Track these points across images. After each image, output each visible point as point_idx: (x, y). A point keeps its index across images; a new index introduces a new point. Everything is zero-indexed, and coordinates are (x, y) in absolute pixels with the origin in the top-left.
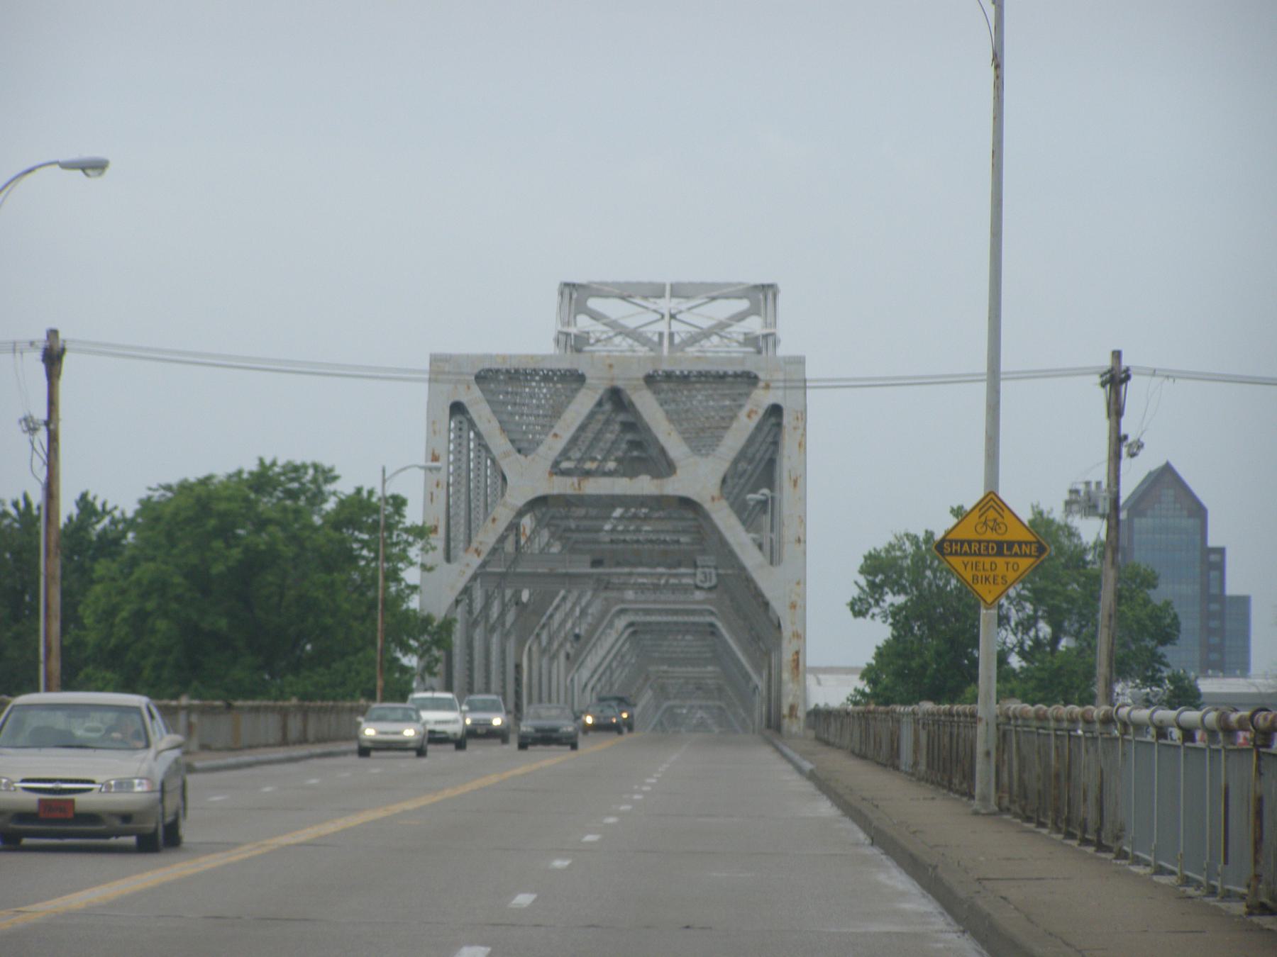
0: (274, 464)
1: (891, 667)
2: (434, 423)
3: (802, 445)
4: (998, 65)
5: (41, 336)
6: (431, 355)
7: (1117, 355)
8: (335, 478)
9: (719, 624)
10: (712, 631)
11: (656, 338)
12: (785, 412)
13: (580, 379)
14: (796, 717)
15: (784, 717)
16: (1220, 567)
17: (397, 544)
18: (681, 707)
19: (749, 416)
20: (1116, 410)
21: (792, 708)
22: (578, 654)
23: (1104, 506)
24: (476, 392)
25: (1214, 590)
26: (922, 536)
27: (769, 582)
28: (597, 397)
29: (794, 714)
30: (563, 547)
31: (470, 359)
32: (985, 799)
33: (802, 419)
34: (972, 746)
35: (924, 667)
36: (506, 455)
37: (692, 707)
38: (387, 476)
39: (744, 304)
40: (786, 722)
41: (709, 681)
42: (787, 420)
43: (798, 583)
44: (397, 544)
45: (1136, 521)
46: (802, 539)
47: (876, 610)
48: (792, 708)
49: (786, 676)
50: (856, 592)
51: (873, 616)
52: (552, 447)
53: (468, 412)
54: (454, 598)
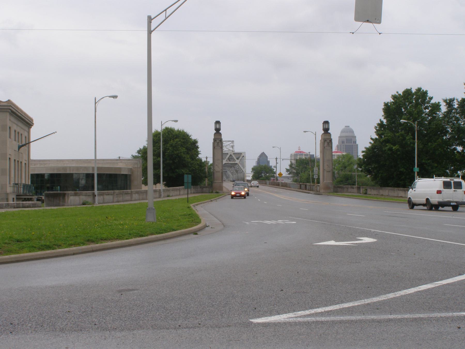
5: (206, 157)
7: (276, 157)
13: (228, 154)
16: (269, 163)
20: (276, 161)
23: (276, 167)
25: (269, 165)
34: (128, 160)
38: (162, 124)
39: (231, 142)
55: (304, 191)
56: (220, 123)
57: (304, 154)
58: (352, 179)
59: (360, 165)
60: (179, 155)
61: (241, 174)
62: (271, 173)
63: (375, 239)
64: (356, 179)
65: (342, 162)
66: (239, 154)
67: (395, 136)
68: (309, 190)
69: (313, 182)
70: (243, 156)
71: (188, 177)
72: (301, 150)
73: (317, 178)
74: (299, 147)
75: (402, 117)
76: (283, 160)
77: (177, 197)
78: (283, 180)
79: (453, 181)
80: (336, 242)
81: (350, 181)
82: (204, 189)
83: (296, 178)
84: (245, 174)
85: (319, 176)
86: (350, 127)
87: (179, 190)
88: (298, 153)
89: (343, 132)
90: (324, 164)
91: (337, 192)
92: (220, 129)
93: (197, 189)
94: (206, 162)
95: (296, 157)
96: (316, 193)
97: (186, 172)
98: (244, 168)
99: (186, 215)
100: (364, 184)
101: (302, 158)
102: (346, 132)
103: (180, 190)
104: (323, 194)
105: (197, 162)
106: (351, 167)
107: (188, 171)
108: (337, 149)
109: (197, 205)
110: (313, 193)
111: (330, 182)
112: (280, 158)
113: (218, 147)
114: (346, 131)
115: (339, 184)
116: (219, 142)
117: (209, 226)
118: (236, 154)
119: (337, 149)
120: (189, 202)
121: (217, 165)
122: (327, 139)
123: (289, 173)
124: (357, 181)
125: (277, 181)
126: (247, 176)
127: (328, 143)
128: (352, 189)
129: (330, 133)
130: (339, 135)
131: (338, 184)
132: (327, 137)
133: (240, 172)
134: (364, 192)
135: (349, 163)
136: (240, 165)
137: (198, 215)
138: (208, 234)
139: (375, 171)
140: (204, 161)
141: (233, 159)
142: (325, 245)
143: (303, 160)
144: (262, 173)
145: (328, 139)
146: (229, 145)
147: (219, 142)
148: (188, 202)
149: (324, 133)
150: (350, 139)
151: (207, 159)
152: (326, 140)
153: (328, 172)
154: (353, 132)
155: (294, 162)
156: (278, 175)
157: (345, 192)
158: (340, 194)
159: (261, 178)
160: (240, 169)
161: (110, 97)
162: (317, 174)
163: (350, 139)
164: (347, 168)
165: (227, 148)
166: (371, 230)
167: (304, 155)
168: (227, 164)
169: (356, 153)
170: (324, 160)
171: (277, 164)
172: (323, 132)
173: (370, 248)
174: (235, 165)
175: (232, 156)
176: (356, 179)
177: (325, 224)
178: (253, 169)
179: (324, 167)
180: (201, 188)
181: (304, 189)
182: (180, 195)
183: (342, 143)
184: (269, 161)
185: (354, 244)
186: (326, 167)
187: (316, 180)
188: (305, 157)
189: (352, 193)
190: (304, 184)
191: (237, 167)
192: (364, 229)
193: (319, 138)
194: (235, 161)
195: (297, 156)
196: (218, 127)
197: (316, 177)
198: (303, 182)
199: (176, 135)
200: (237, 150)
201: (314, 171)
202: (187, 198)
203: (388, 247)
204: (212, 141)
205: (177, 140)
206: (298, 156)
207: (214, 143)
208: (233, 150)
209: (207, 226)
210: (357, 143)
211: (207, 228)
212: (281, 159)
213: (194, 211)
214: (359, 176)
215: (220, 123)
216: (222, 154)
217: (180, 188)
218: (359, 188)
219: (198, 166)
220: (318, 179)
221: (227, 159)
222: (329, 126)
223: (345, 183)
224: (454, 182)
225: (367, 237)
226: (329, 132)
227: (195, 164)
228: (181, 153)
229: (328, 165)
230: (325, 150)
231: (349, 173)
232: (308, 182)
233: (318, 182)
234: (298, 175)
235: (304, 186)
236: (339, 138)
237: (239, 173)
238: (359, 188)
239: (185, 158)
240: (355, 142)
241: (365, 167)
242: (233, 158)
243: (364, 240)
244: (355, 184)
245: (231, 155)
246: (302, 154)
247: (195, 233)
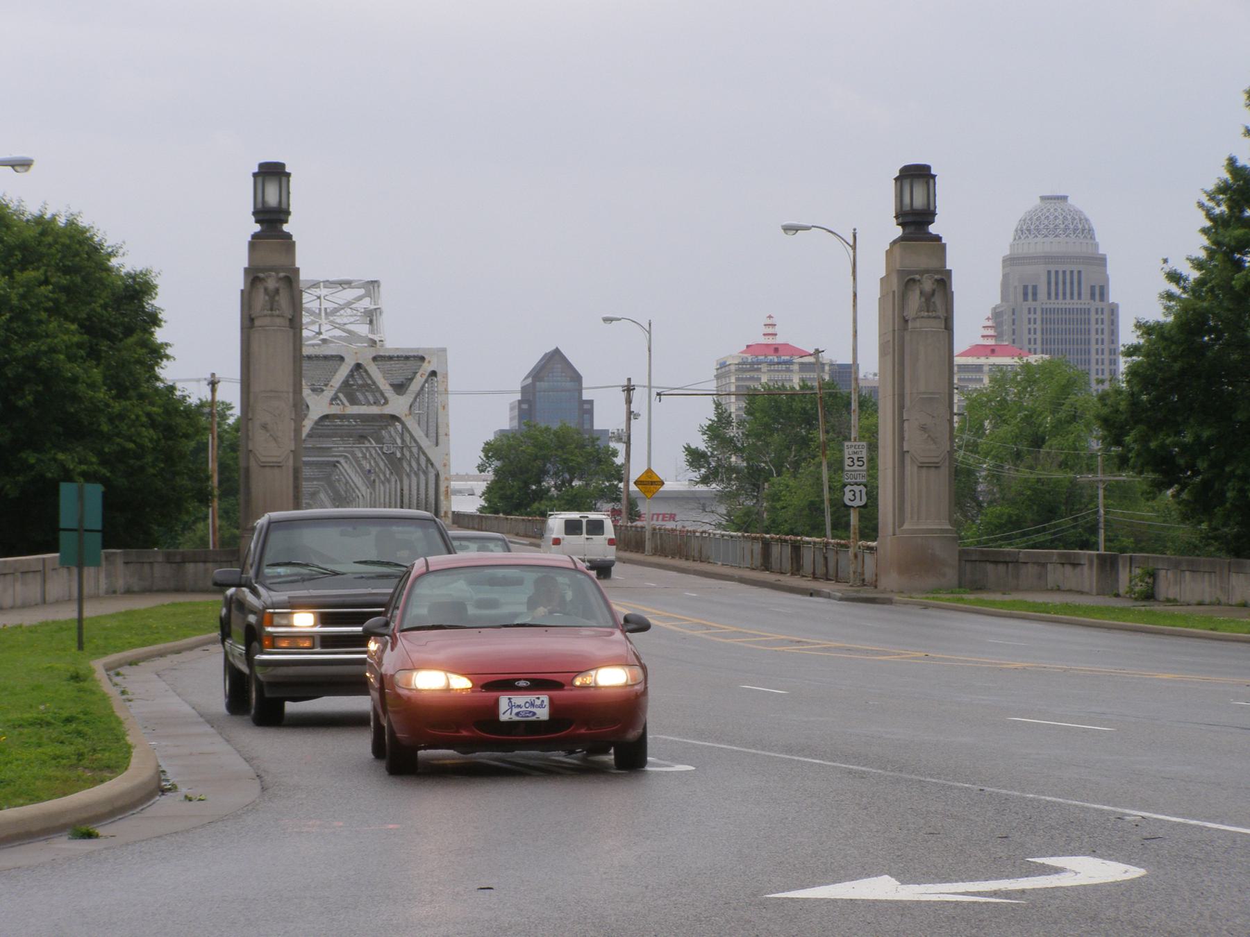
4: (650, 351)
5: (208, 376)
7: (629, 380)
8: (232, 408)
11: (317, 311)
13: (342, 359)
16: (590, 412)
23: (625, 439)
25: (587, 426)
27: (433, 453)
28: (350, 368)
32: (648, 551)
35: (513, 494)
39: (362, 291)
45: (538, 383)
47: (489, 469)
50: (480, 461)
52: (329, 393)
55: (788, 580)
56: (288, 175)
57: (801, 364)
58: (1081, 510)
59: (1114, 428)
60: (44, 363)
61: (422, 477)
62: (596, 473)
63: (1136, 865)
64: (1102, 511)
65: (1021, 408)
66: (407, 358)
68: (815, 577)
69: (841, 525)
70: (434, 373)
71: (81, 496)
72: (779, 340)
73: (865, 506)
74: (769, 321)
76: (659, 394)
77: (30, 618)
78: (672, 517)
79: (586, 519)
80: (903, 883)
81: (1066, 522)
82: (190, 567)
83: (749, 503)
84: (442, 478)
85: (872, 496)
86: (1070, 201)
87: (39, 577)
88: (761, 358)
89: (1026, 229)
90: (902, 422)
91: (978, 587)
92: (288, 213)
93: (147, 568)
94: (213, 410)
95: (752, 379)
96: (855, 595)
97: (84, 467)
98: (437, 444)
99: (49, 724)
100: (1148, 542)
101: (787, 385)
102: (1044, 232)
103: (43, 574)
104: (897, 598)
105: (149, 408)
106: (1071, 437)
107: (94, 460)
108: (991, 332)
109: (133, 663)
110: (839, 595)
111: (942, 531)
112: (650, 387)
113: (272, 316)
114: (1047, 227)
115: (1001, 539)
116: (277, 291)
117: (173, 788)
118: (391, 358)
119: (991, 332)
120: (86, 645)
121: (264, 427)
122: (922, 272)
123: (703, 471)
124: (1106, 521)
125: (632, 520)
126: (459, 492)
127: (928, 298)
128: (1068, 569)
129: (938, 238)
130: (1007, 252)
131: (996, 540)
132: (920, 259)
133: (414, 465)
134: (1137, 589)
135: (1062, 415)
136: (411, 424)
137: (120, 723)
138: (159, 837)
139: (1202, 465)
140: (202, 405)
141: (372, 392)
142: (835, 901)
143: (792, 396)
144: (546, 473)
145: (927, 271)
146: (348, 304)
147: (277, 291)
148: (81, 646)
149: (902, 239)
150: (1076, 274)
151: (213, 391)
152: (917, 277)
153: (924, 470)
154: (1091, 230)
155: (739, 409)
156: (635, 483)
157: (1031, 589)
158: (998, 597)
159: (536, 505)
160: (415, 450)
162: (864, 480)
163: (1076, 274)
164: (1050, 447)
165: (341, 327)
166: (1127, 811)
167: (796, 367)
168: (338, 422)
169: (1106, 356)
170: (902, 396)
171: (633, 421)
172: (899, 231)
173: (1093, 919)
174: (382, 428)
175: (366, 371)
176: (1102, 511)
177: (862, 776)
178: (491, 450)
179: (902, 439)
180: (169, 559)
181: (789, 567)
182: (44, 602)
183: (1025, 295)
184: (591, 402)
185: (1007, 894)
186: (914, 441)
187: (854, 519)
188: (803, 380)
189: (1070, 591)
190: (786, 541)
191: (399, 441)
192: (1083, 809)
193: (874, 266)
194: (383, 401)
195: (755, 375)
196: (272, 198)
197: (854, 497)
198: (786, 527)
199: (23, 247)
200: (395, 338)
201: (848, 462)
202: (75, 624)
203: (1201, 915)
204: (239, 282)
205: (31, 274)
206: (759, 370)
207: (247, 298)
208: (376, 338)
209: (163, 791)
210: (1113, 297)
211: (160, 800)
212: (654, 392)
213: (105, 698)
214: (1118, 493)
215: (288, 175)
216: (298, 358)
217: (44, 560)
218: (1108, 565)
219: (151, 431)
220: (869, 511)
221: (340, 390)
222: (930, 195)
223: (1038, 531)
224: (587, 521)
225: (1093, 853)
226: (933, 229)
227: (133, 417)
228: (53, 350)
229: (923, 428)
230: (907, 338)
231: (1058, 475)
232: (817, 529)
233: (870, 529)
234: (757, 487)
235: (788, 550)
236: (1004, 267)
237: (408, 475)
238: (1108, 565)
239: (75, 380)
240: (1100, 292)
241: (1144, 439)
242: (374, 383)
243: (1070, 871)
244: (1093, 539)
245: (358, 366)
246: (785, 363)
247: (84, 828)
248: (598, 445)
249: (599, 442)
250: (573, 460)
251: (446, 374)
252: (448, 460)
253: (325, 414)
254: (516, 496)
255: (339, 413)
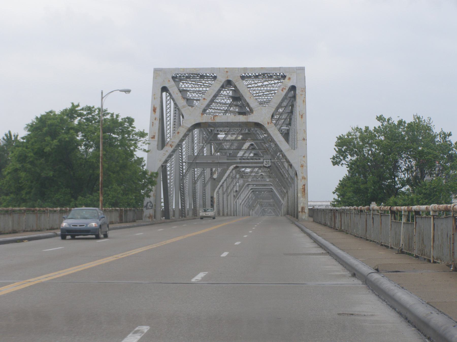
0: (78, 106)
1: (351, 188)
2: (154, 95)
3: (304, 101)
6: (154, 69)
9: (273, 188)
10: (272, 191)
12: (297, 89)
14: (304, 212)
15: (299, 212)
17: (132, 140)
18: (266, 209)
19: (282, 90)
21: (303, 208)
22: (237, 195)
24: (172, 83)
26: (364, 129)
27: (292, 156)
28: (221, 84)
29: (304, 210)
30: (240, 176)
31: (171, 70)
33: (304, 91)
36: (184, 107)
37: (268, 209)
38: (103, 96)
40: (300, 214)
41: (271, 203)
42: (298, 91)
43: (304, 157)
44: (132, 140)
46: (305, 139)
47: (343, 162)
48: (303, 208)
49: (299, 195)
50: (335, 153)
51: (342, 164)
53: (169, 91)
54: (161, 164)
67: (376, 152)
75: (145, 214)
161: (121, 91)
248: (450, 141)
249: (450, 138)
250: (429, 153)
251: (305, 88)
252: (306, 162)
253: (197, 122)
254: (370, 190)
255: (210, 121)
